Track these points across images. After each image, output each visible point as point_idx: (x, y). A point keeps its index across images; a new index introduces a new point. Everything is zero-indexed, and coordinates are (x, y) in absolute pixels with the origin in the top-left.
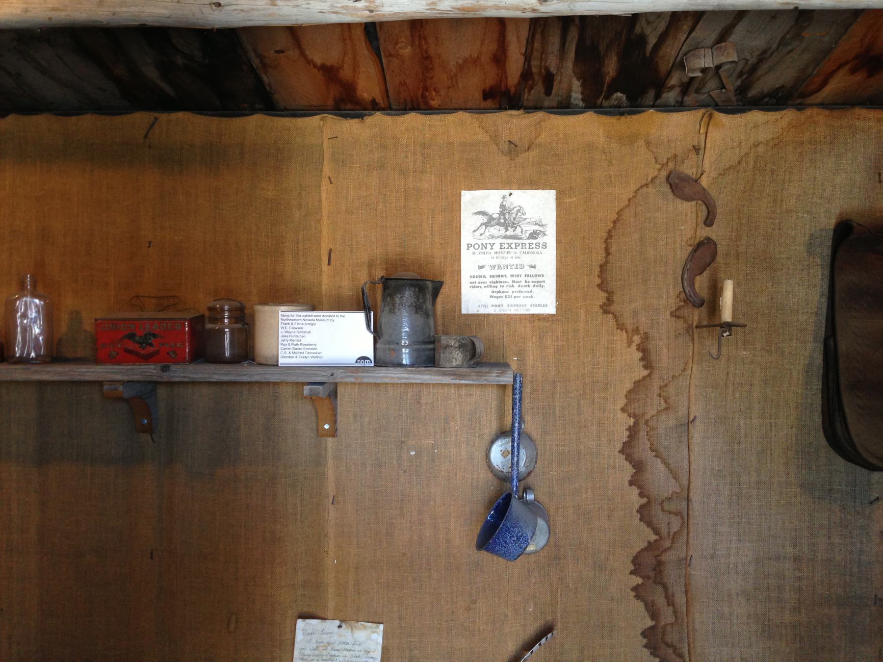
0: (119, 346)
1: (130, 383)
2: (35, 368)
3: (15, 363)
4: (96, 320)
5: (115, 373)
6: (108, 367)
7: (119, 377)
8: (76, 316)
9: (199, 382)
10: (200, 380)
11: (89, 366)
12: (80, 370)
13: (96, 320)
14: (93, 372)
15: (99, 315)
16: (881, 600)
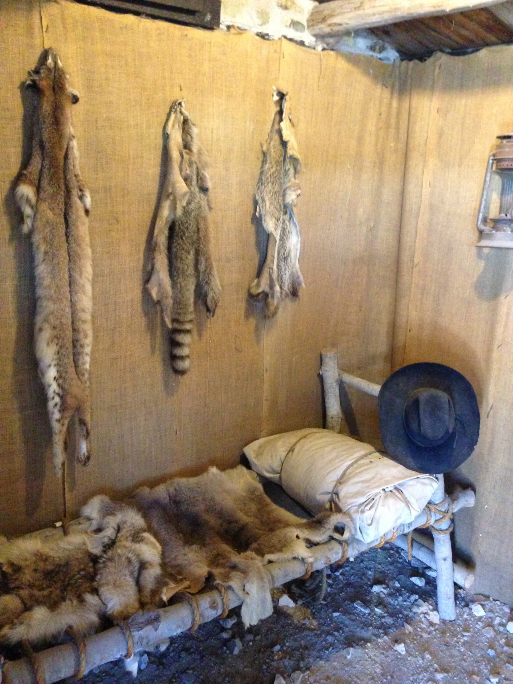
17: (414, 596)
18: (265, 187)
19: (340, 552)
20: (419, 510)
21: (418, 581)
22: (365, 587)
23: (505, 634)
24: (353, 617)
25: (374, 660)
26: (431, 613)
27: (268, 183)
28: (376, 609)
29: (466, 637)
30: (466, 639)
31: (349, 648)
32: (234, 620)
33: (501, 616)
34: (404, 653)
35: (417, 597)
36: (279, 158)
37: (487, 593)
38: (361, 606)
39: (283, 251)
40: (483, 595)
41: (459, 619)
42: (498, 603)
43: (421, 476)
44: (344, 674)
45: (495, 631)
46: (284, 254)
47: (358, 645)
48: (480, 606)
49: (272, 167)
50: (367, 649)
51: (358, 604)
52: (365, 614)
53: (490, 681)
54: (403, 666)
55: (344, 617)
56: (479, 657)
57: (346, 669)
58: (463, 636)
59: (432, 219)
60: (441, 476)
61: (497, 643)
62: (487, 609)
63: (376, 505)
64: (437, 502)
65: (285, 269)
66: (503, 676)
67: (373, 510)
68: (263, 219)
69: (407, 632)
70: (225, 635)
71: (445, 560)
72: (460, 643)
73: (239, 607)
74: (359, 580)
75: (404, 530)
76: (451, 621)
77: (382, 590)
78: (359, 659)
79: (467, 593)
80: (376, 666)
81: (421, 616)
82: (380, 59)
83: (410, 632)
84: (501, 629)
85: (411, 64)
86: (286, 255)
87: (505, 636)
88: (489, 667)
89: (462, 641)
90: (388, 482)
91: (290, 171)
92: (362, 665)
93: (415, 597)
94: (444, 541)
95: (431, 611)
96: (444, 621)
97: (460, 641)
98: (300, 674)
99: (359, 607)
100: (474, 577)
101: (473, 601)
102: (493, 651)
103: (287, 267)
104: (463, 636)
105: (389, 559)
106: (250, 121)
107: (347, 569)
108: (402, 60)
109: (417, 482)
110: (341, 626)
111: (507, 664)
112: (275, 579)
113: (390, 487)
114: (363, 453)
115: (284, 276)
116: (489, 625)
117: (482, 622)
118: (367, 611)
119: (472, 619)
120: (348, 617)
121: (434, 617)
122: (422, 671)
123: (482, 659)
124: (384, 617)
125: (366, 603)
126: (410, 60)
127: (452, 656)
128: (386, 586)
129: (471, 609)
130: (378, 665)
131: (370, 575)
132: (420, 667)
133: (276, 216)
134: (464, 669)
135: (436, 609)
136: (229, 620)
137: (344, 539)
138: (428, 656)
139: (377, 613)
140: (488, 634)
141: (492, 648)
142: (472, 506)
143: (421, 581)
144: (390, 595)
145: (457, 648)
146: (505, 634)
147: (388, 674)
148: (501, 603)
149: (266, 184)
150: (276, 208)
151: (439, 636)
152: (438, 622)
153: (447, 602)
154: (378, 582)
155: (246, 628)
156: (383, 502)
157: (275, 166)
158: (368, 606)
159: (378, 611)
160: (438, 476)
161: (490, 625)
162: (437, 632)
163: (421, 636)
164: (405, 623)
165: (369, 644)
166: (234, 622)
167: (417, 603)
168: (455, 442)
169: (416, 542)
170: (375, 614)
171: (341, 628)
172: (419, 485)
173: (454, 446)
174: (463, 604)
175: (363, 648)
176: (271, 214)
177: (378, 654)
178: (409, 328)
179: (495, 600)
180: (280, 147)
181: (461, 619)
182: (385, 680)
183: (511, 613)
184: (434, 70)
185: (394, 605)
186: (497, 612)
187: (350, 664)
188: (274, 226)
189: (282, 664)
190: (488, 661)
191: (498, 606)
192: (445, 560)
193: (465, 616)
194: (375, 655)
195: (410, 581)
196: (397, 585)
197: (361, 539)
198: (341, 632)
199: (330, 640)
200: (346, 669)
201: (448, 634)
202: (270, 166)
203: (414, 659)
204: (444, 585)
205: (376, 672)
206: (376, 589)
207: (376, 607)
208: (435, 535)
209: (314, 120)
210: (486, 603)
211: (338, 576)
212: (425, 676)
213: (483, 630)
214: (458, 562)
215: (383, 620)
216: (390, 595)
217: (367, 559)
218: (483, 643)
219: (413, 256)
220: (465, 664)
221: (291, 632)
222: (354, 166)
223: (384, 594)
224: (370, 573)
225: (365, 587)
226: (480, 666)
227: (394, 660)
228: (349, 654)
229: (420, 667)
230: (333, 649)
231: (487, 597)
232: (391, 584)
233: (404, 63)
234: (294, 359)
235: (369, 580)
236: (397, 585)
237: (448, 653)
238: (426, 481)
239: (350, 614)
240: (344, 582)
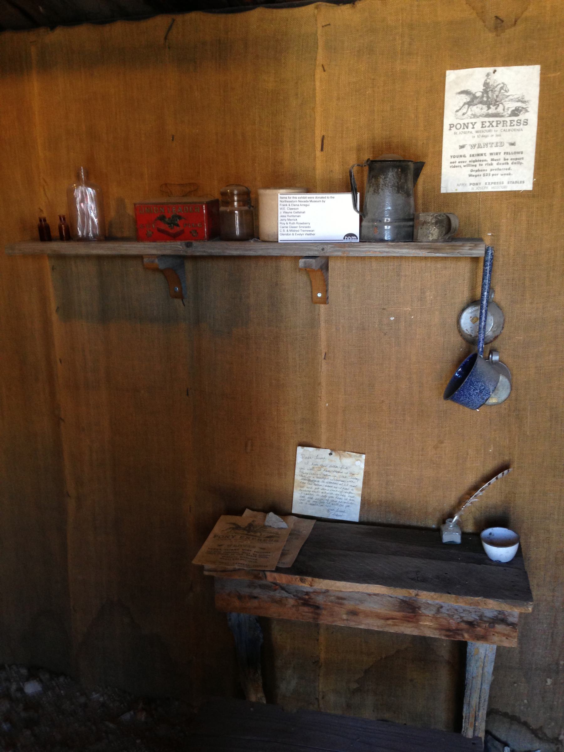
2: (93, 245)
4: (135, 204)
7: (154, 252)
125: (383, 444)
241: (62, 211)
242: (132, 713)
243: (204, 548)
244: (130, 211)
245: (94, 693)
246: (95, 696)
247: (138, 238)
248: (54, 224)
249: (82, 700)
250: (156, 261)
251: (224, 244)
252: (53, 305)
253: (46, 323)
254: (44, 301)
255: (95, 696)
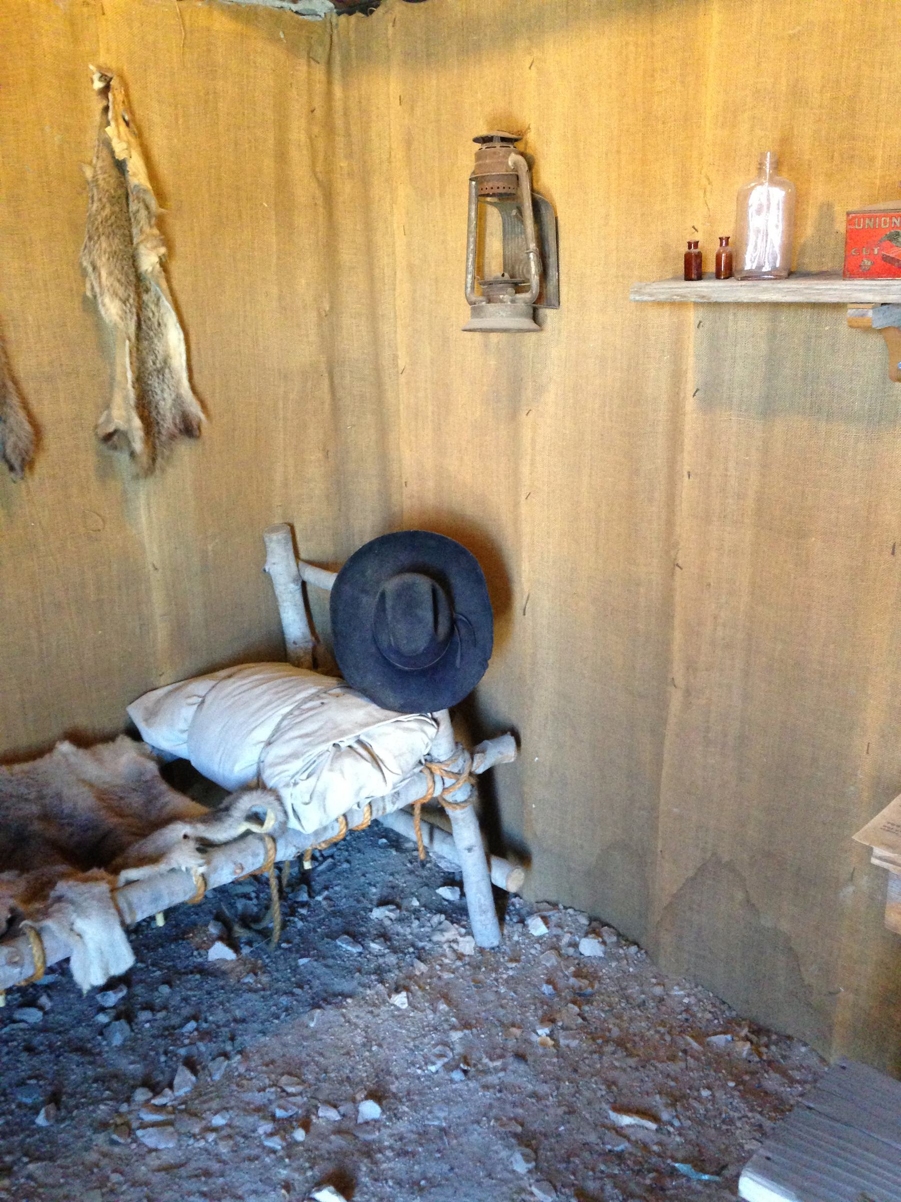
0: (876, 252)
1: (885, 307)
2: (764, 284)
3: (743, 279)
4: (848, 214)
5: (864, 291)
6: (856, 282)
7: (869, 297)
8: (827, 210)
9: (242, 663)
10: (239, 667)
11: (833, 282)
12: (817, 287)
13: (848, 214)
14: (835, 290)
15: (855, 207)
16: (657, 1189)
17: (438, 916)
18: (95, 243)
19: (262, 852)
20: (400, 772)
21: (446, 892)
22: (362, 912)
23: (577, 958)
24: (330, 962)
25: (355, 1024)
26: (460, 939)
27: (99, 237)
28: (373, 945)
29: (511, 970)
30: (511, 973)
31: (313, 1011)
32: (121, 990)
33: (573, 931)
34: (405, 1006)
35: (443, 917)
36: (115, 191)
37: (553, 899)
38: (348, 943)
39: (153, 357)
40: (548, 902)
41: (505, 944)
42: (570, 911)
43: (403, 718)
44: (301, 1051)
45: (560, 955)
46: (154, 363)
47: (329, 1003)
48: (539, 919)
49: (103, 208)
50: (345, 1008)
51: (343, 941)
52: (352, 955)
53: (537, 1034)
54: (400, 1028)
55: (315, 964)
56: (529, 999)
57: (305, 1044)
58: (507, 969)
59: (415, 291)
60: (442, 715)
61: (560, 974)
62: (552, 924)
63: (318, 772)
64: (442, 759)
65: (162, 391)
66: (560, 1024)
67: (313, 779)
68: (100, 301)
69: (418, 973)
70: (102, 1018)
71: (470, 850)
72: (500, 980)
73: (67, 960)
74: (354, 903)
75: (384, 809)
76: (493, 948)
77: (387, 913)
78: (329, 1025)
79: (525, 901)
80: (356, 1032)
81: (445, 946)
82: (297, 12)
83: (422, 974)
84: (571, 951)
85: (353, 18)
86: (158, 366)
87: (576, 962)
88: (540, 1012)
89: (505, 976)
90: (343, 733)
91: (139, 215)
92: (333, 1035)
93: (436, 919)
94: (463, 820)
95: (461, 936)
96: (481, 950)
97: (501, 978)
98: (221, 1063)
99: (344, 946)
100: (523, 874)
101: (530, 914)
102: (550, 987)
103: (165, 387)
104: (507, 969)
105: (409, 865)
106: (52, 127)
107: (337, 888)
108: (339, 14)
109: (397, 728)
110: (309, 977)
111: (570, 1005)
112: (134, 906)
113: (347, 741)
114: (313, 690)
115: (162, 403)
116: (552, 948)
117: (541, 944)
118: (355, 950)
119: (527, 941)
120: (324, 962)
121: (467, 946)
122: (430, 1031)
123: (532, 1001)
124: (383, 956)
125: (356, 937)
126: (350, 13)
127: (484, 1003)
128: (394, 907)
129: (525, 926)
130: (359, 1031)
131: (374, 894)
132: (427, 1026)
133: (121, 295)
134: (499, 1021)
135: (470, 933)
136: (110, 993)
137: (268, 831)
138: (443, 1007)
139: (373, 951)
140: (548, 961)
141: (643, 993)
142: (513, 760)
143: (453, 893)
144: (400, 920)
145: (495, 989)
146: (577, 958)
147: (374, 1043)
148: (575, 910)
149: (96, 238)
150: (119, 281)
151: (468, 973)
152: (472, 953)
153: (483, 918)
154: (383, 902)
155: (85, 992)
156: (331, 765)
157: (108, 205)
158: (360, 943)
159: (375, 947)
160: (437, 715)
161: (556, 948)
162: (467, 967)
163: (440, 978)
164: (416, 960)
165: (349, 1000)
166: (121, 995)
167: (442, 927)
168: (459, 657)
169: (438, 828)
170: (370, 953)
171: (308, 982)
172: (400, 733)
173: (458, 661)
174: (515, 920)
175: (337, 1008)
176: (111, 291)
177: (362, 1015)
178: (404, 481)
179: (565, 908)
180: (115, 172)
181: (508, 943)
182: (367, 1054)
183: (589, 925)
184: (386, 29)
185: (405, 935)
186: (568, 926)
187: (314, 1034)
188: (120, 312)
189: (196, 1051)
190: (542, 1002)
191: (571, 916)
192: (470, 850)
193: (516, 938)
194: (357, 1017)
195: (437, 895)
196: (415, 903)
197: (298, 827)
198: (306, 987)
199: (285, 1003)
200: (305, 1044)
201: (483, 969)
202: (101, 206)
203: (419, 1015)
204: (474, 891)
205: (354, 1043)
206: (378, 913)
207: (373, 941)
208: (449, 811)
209: (180, 122)
210: (550, 913)
211: (320, 902)
212: (432, 1038)
213: (541, 957)
214: (510, 858)
215: (381, 960)
216: (400, 920)
217: (372, 870)
218: (538, 976)
219: (395, 357)
220: (502, 1012)
221: (221, 999)
222: (276, 204)
223: (391, 920)
224: (374, 890)
225: (362, 912)
226: (526, 1012)
227: (387, 1020)
228: (312, 1019)
229: (427, 1026)
230: (286, 1016)
231: (555, 905)
232: (405, 903)
233: (343, 18)
234: (210, 548)
235: (371, 901)
236: (415, 903)
237: (478, 998)
238: (414, 725)
239: (324, 958)
240: (329, 910)
241: (726, 230)
242: (729, 1037)
243: (879, 819)
244: (841, 226)
245: (676, 988)
246: (677, 992)
247: (850, 272)
248: (710, 250)
249: (658, 990)
250: (870, 313)
251: (500, 233)
252: (691, 381)
253: (676, 411)
254: (677, 376)
255: (677, 992)
